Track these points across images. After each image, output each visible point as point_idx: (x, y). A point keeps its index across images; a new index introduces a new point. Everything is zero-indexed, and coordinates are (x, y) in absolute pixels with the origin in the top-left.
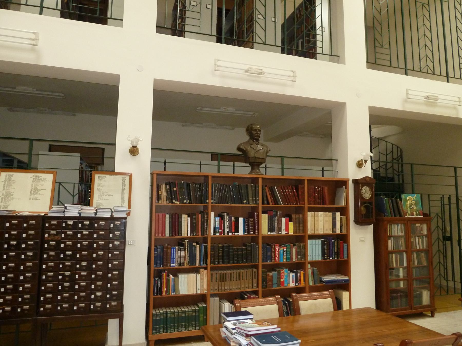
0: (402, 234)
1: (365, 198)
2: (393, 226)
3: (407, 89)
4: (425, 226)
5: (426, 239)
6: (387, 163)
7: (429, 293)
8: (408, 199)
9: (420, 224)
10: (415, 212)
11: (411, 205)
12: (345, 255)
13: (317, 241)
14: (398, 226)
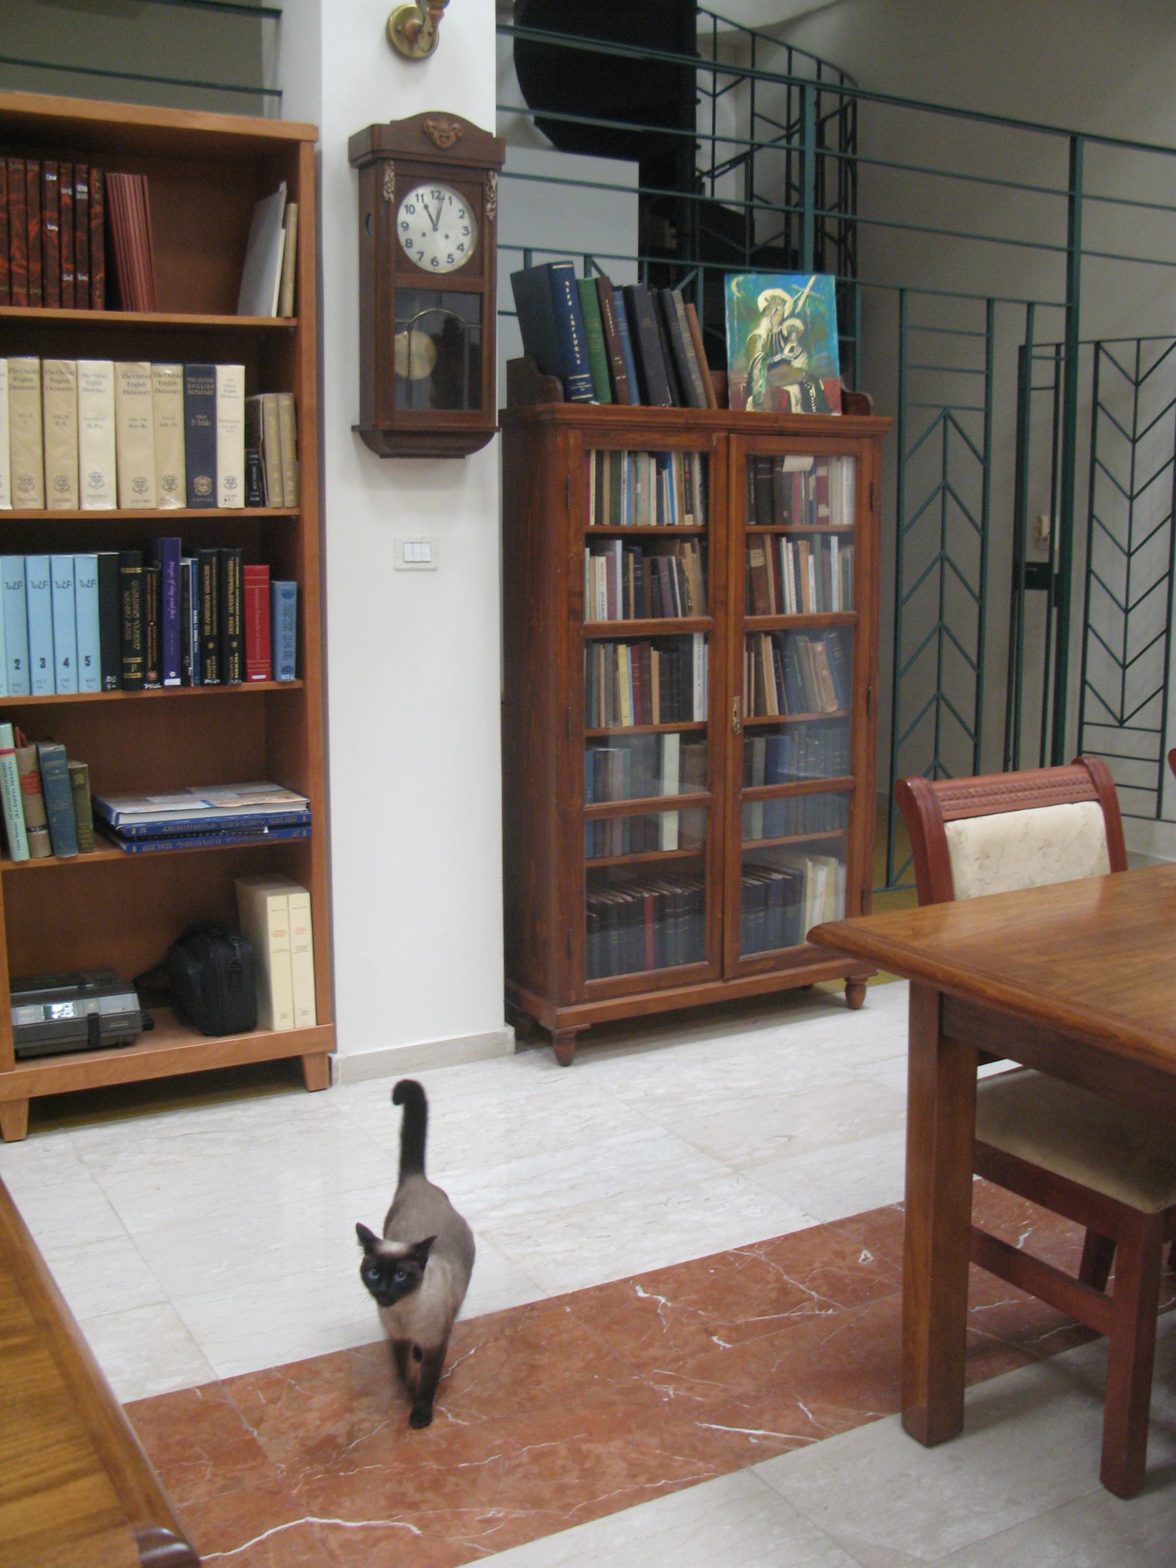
0: (689, 520)
1: (425, 264)
2: (625, 464)
4: (843, 477)
5: (849, 552)
6: (756, 147)
7: (842, 872)
8: (761, 303)
9: (806, 462)
11: (775, 343)
12: (285, 657)
13: (62, 562)
14: (662, 465)
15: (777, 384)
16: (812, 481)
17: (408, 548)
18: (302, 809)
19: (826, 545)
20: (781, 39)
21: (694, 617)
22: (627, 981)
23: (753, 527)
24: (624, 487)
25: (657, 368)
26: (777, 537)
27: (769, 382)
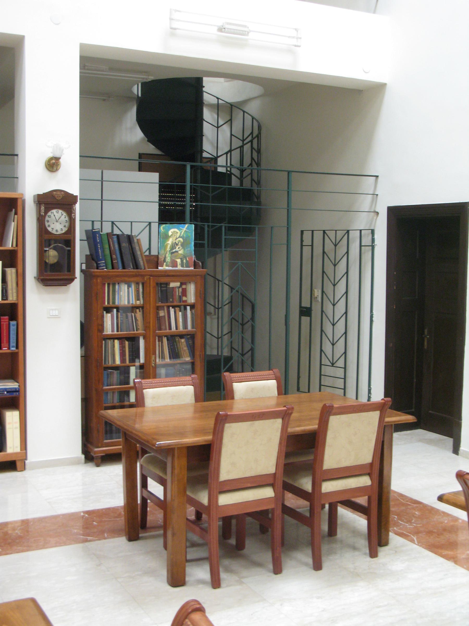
0: (138, 302)
1: (54, 232)
2: (117, 287)
3: (171, 9)
8: (170, 233)
9: (178, 284)
10: (179, 261)
11: (174, 245)
14: (129, 287)
15: (173, 259)
16: (180, 290)
17: (51, 312)
18: (17, 387)
19: (185, 309)
20: (241, 108)
21: (140, 332)
22: (115, 442)
23: (160, 304)
24: (117, 293)
25: (128, 258)
26: (168, 307)
27: (171, 258)
